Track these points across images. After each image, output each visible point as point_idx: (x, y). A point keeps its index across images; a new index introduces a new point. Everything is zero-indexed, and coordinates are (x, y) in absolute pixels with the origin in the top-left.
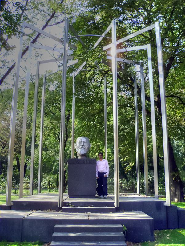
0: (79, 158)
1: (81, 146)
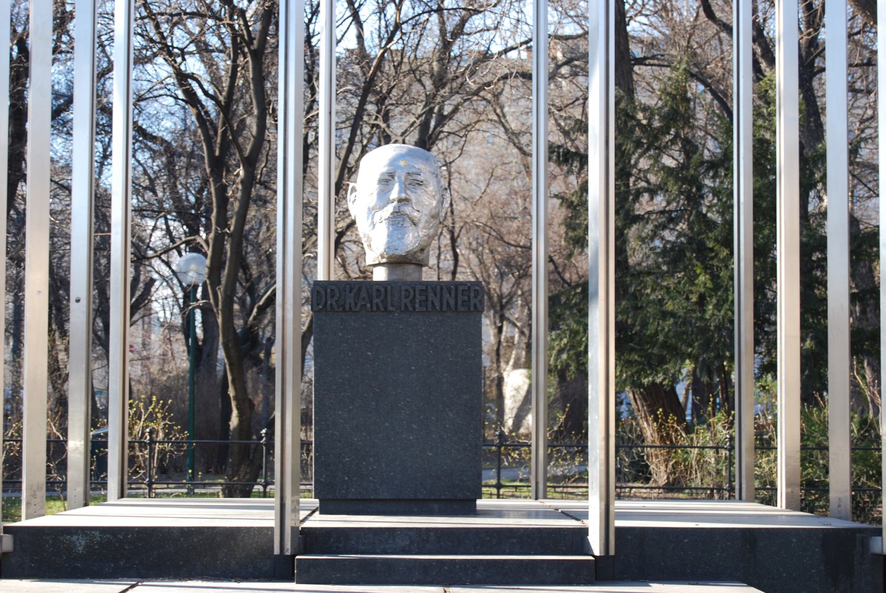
0: (380, 275)
1: (390, 209)
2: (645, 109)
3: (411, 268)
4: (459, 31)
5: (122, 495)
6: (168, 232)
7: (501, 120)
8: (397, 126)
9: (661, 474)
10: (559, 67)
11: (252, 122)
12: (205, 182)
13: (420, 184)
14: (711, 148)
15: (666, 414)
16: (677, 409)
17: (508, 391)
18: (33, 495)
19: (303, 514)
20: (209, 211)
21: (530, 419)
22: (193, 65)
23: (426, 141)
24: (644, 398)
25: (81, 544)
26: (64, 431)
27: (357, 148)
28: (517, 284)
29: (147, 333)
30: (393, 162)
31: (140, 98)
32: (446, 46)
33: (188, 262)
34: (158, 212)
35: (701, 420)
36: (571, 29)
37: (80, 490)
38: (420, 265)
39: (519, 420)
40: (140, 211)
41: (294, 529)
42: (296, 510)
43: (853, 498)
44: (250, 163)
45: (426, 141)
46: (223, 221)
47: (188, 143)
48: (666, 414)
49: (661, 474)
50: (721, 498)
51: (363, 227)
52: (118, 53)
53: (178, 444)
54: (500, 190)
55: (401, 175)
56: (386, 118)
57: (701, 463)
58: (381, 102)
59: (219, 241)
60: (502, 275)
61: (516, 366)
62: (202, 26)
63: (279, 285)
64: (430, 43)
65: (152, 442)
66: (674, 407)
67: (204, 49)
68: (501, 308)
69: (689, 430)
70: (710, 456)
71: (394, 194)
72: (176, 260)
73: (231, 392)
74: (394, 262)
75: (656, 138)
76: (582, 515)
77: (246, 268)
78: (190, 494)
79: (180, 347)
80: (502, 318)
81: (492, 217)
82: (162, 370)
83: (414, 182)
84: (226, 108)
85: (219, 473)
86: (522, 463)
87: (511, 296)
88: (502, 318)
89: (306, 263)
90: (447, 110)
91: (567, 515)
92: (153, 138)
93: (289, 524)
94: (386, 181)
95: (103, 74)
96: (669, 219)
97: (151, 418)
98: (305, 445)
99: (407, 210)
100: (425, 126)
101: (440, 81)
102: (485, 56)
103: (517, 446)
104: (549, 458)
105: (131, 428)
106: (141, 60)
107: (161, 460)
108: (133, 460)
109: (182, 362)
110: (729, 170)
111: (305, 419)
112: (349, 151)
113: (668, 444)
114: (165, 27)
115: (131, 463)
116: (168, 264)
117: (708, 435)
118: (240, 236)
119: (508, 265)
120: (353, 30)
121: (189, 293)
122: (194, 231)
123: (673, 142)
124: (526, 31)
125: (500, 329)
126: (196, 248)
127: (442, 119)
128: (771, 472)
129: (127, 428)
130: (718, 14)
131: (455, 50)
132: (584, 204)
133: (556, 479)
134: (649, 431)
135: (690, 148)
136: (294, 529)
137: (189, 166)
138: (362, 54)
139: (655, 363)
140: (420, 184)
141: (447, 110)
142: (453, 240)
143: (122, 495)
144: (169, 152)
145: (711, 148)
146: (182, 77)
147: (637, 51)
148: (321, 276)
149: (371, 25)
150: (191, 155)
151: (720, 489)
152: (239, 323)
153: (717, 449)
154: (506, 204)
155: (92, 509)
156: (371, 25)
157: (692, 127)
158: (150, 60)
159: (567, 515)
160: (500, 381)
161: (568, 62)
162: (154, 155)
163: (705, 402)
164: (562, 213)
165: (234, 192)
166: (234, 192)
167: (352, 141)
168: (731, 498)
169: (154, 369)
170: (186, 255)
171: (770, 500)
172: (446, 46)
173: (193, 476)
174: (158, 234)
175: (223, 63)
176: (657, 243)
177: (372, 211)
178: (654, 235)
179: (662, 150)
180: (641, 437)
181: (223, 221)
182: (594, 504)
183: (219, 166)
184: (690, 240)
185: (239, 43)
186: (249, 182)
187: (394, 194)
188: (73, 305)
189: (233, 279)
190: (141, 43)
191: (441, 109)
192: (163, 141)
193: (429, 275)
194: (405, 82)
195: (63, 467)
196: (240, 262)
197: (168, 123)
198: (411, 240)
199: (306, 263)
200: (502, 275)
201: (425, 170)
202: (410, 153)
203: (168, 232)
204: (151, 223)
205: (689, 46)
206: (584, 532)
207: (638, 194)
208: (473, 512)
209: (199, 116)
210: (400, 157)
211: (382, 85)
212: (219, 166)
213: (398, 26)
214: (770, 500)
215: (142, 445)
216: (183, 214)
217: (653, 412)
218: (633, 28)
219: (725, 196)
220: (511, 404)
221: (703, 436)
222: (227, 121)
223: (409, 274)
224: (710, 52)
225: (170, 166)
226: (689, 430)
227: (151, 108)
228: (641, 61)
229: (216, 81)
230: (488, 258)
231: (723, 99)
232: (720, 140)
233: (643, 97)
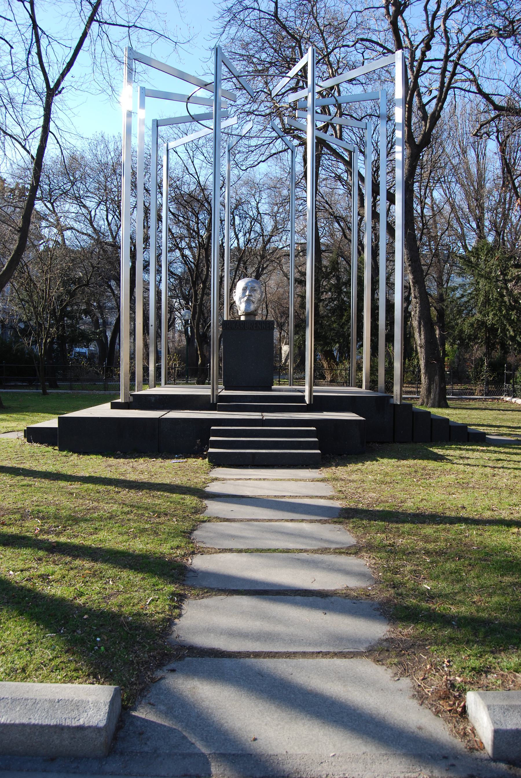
0: (243, 318)
1: (246, 298)
2: (325, 267)
3: (252, 316)
4: (269, 241)
5: (166, 384)
6: (180, 303)
7: (281, 269)
8: (250, 270)
9: (329, 378)
10: (299, 253)
11: (205, 269)
12: (191, 289)
13: (255, 290)
14: (344, 279)
15: (330, 360)
16: (334, 358)
17: (283, 352)
18: (139, 384)
19: (219, 390)
20: (192, 297)
21: (289, 361)
22: (187, 252)
23: (257, 277)
24: (324, 355)
25: (153, 399)
26: (148, 363)
27: (237, 278)
28: (286, 319)
29: (174, 333)
30: (247, 284)
31: (171, 263)
32: (265, 247)
33: (186, 312)
34: (177, 297)
35: (341, 362)
36: (303, 241)
37: (153, 383)
38: (255, 315)
39: (286, 360)
40: (171, 297)
41: (217, 395)
42: (217, 389)
43: (386, 386)
44: (204, 283)
45: (257, 277)
46: (196, 300)
47: (186, 276)
48: (330, 360)
49: (329, 378)
50: (347, 386)
51: (237, 303)
52: (163, 248)
53: (183, 368)
54: (281, 290)
55: (249, 287)
56: (246, 269)
57: (341, 375)
58: (245, 263)
59: (195, 307)
60: (281, 317)
61: (285, 344)
62: (190, 241)
63: (212, 321)
64: (259, 246)
65: (175, 367)
66: (333, 358)
67: (190, 248)
68: (281, 326)
69: (337, 364)
70: (344, 373)
71: (247, 294)
72: (183, 312)
73: (199, 353)
74: (247, 314)
75: (328, 275)
76: (303, 391)
77: (203, 314)
78: (187, 383)
79: (184, 338)
80: (281, 329)
81: (279, 298)
82: (179, 345)
83: (253, 290)
84: (197, 266)
85: (195, 377)
86: (286, 374)
87: (284, 323)
88: (281, 329)
89: (220, 314)
90: (265, 266)
91: (299, 391)
92: (175, 275)
93: (215, 394)
94: (245, 290)
95: (158, 257)
96: (332, 300)
97: (174, 360)
98: (220, 368)
99: (251, 298)
100: (258, 271)
101: (263, 257)
102: (276, 249)
103: (285, 369)
104: (294, 373)
105: (168, 363)
106: (171, 250)
107: (178, 373)
108: (169, 373)
109: (185, 343)
110: (350, 285)
111: (220, 360)
112: (234, 279)
113: (331, 369)
114: (178, 240)
115: (168, 374)
116: (180, 313)
117: (343, 366)
118: (201, 304)
119: (283, 313)
120: (236, 241)
121: (186, 322)
122: (187, 303)
123: (334, 276)
124: (289, 242)
125: (281, 333)
126: (188, 309)
127: (263, 269)
128: (362, 377)
129: (167, 364)
130: (348, 237)
131: (268, 247)
132: (305, 297)
133: (297, 379)
134: (325, 365)
135: (338, 278)
136: (217, 395)
137: (186, 283)
138: (238, 248)
139: (327, 344)
140: (255, 290)
141: (265, 266)
142: (267, 306)
143: (166, 384)
144: (180, 278)
145: (344, 279)
146: (183, 255)
147: (323, 248)
148: (225, 319)
149: (242, 240)
150: (187, 280)
151: (346, 382)
152: (201, 331)
153: (346, 370)
154: (283, 295)
155: (157, 388)
156: (242, 240)
157: (339, 272)
158: (174, 251)
159: (299, 391)
160: (281, 348)
161: (302, 251)
162: (176, 280)
163: (342, 356)
164: (299, 299)
165: (200, 292)
166: (200, 292)
167: (235, 276)
168: (349, 386)
169: (176, 345)
170: (185, 310)
171: (361, 387)
172: (265, 247)
173: (188, 378)
174: (176, 304)
175: (195, 250)
176: (328, 308)
177: (240, 299)
178: (327, 305)
179: (330, 279)
180: (323, 366)
181: (196, 300)
182: (307, 388)
183: (195, 284)
184: (338, 306)
185: (201, 246)
186: (204, 288)
187: (247, 294)
188: (150, 327)
189: (199, 318)
190: (208, 183)
191: (263, 265)
192: (178, 275)
193: (258, 318)
194: (252, 258)
195: (148, 375)
196: (201, 312)
197: (179, 270)
198: (252, 307)
199: (220, 314)
200: (281, 317)
201: (256, 286)
202: (252, 281)
203: (180, 303)
204: (175, 300)
205: (339, 247)
206: (304, 396)
207: (322, 293)
208: (271, 390)
209: (189, 268)
210: (249, 282)
211: (245, 259)
212: (195, 284)
213: (249, 240)
214: (361, 387)
215: (172, 369)
216: (184, 298)
217: (326, 359)
218: (322, 241)
219: (348, 294)
220: (284, 356)
221: (341, 366)
222: (197, 270)
223: (252, 318)
224: (346, 248)
225: (180, 283)
226: (337, 364)
227: (175, 265)
228: (324, 251)
229: (194, 257)
230: (277, 311)
231: (349, 263)
232: (150, 541)
233: (325, 262)
